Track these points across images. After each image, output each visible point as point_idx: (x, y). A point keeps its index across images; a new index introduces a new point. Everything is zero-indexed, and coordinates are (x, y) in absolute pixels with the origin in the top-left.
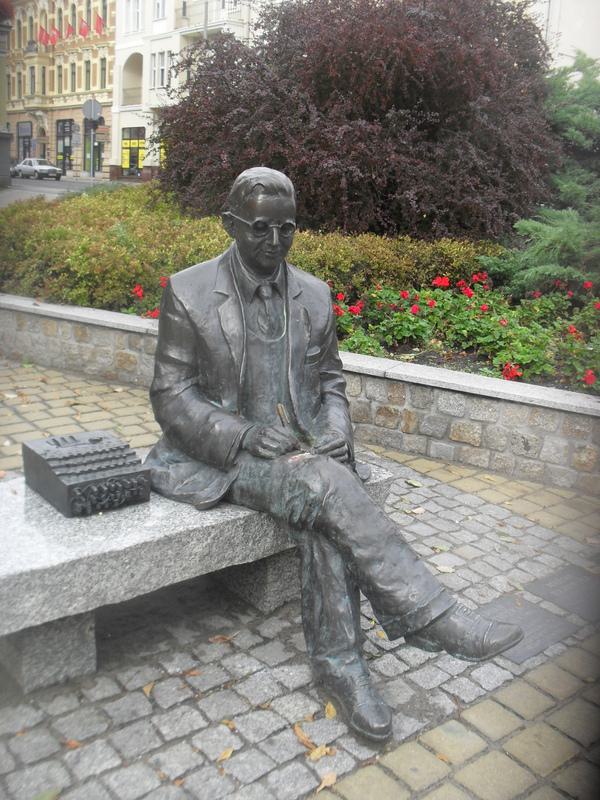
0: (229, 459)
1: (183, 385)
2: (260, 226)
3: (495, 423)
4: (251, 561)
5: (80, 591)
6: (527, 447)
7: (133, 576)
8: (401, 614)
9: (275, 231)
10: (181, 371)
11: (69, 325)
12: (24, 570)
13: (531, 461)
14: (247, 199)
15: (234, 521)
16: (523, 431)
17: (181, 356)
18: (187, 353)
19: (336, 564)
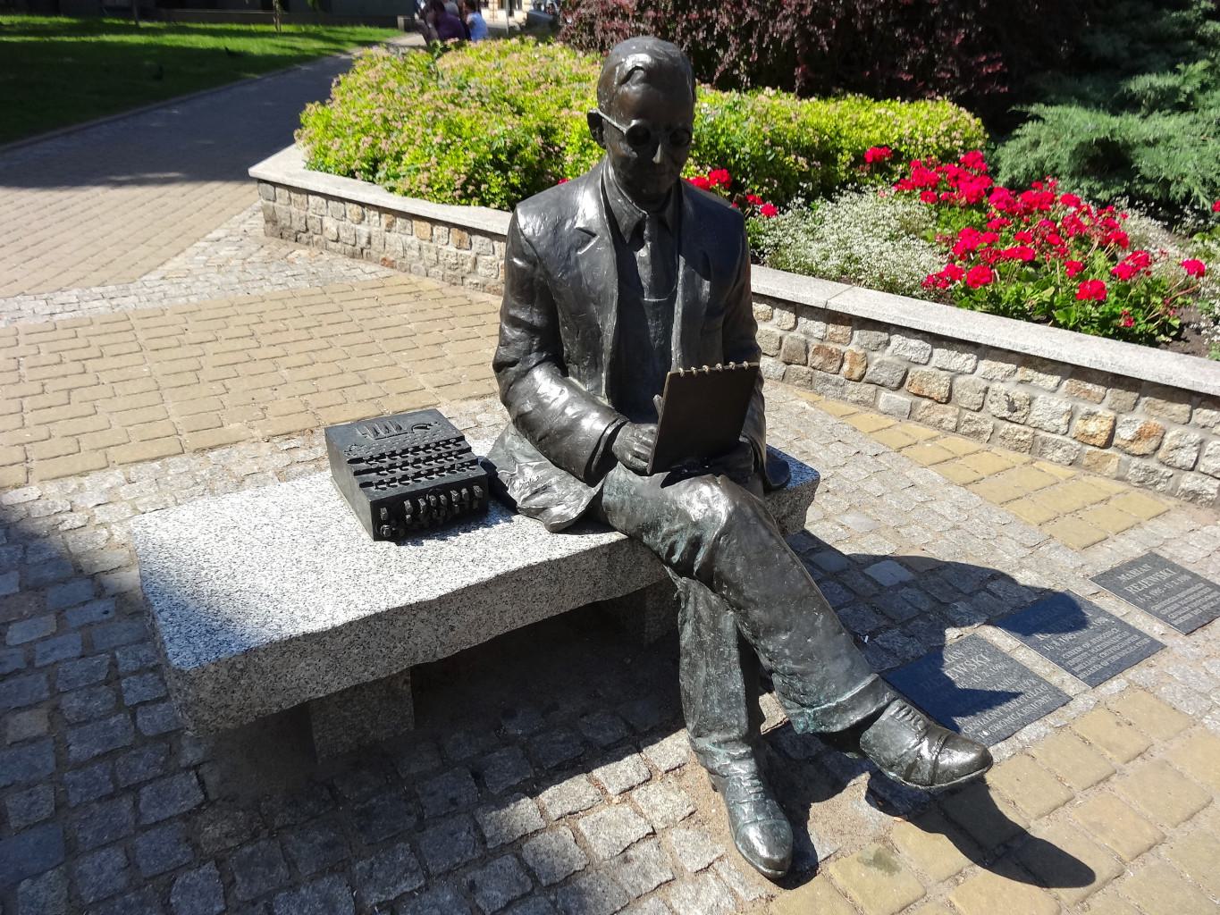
6: (1012, 408)
10: (532, 339)
12: (294, 634)
13: (1015, 425)
14: (620, 92)
18: (539, 314)
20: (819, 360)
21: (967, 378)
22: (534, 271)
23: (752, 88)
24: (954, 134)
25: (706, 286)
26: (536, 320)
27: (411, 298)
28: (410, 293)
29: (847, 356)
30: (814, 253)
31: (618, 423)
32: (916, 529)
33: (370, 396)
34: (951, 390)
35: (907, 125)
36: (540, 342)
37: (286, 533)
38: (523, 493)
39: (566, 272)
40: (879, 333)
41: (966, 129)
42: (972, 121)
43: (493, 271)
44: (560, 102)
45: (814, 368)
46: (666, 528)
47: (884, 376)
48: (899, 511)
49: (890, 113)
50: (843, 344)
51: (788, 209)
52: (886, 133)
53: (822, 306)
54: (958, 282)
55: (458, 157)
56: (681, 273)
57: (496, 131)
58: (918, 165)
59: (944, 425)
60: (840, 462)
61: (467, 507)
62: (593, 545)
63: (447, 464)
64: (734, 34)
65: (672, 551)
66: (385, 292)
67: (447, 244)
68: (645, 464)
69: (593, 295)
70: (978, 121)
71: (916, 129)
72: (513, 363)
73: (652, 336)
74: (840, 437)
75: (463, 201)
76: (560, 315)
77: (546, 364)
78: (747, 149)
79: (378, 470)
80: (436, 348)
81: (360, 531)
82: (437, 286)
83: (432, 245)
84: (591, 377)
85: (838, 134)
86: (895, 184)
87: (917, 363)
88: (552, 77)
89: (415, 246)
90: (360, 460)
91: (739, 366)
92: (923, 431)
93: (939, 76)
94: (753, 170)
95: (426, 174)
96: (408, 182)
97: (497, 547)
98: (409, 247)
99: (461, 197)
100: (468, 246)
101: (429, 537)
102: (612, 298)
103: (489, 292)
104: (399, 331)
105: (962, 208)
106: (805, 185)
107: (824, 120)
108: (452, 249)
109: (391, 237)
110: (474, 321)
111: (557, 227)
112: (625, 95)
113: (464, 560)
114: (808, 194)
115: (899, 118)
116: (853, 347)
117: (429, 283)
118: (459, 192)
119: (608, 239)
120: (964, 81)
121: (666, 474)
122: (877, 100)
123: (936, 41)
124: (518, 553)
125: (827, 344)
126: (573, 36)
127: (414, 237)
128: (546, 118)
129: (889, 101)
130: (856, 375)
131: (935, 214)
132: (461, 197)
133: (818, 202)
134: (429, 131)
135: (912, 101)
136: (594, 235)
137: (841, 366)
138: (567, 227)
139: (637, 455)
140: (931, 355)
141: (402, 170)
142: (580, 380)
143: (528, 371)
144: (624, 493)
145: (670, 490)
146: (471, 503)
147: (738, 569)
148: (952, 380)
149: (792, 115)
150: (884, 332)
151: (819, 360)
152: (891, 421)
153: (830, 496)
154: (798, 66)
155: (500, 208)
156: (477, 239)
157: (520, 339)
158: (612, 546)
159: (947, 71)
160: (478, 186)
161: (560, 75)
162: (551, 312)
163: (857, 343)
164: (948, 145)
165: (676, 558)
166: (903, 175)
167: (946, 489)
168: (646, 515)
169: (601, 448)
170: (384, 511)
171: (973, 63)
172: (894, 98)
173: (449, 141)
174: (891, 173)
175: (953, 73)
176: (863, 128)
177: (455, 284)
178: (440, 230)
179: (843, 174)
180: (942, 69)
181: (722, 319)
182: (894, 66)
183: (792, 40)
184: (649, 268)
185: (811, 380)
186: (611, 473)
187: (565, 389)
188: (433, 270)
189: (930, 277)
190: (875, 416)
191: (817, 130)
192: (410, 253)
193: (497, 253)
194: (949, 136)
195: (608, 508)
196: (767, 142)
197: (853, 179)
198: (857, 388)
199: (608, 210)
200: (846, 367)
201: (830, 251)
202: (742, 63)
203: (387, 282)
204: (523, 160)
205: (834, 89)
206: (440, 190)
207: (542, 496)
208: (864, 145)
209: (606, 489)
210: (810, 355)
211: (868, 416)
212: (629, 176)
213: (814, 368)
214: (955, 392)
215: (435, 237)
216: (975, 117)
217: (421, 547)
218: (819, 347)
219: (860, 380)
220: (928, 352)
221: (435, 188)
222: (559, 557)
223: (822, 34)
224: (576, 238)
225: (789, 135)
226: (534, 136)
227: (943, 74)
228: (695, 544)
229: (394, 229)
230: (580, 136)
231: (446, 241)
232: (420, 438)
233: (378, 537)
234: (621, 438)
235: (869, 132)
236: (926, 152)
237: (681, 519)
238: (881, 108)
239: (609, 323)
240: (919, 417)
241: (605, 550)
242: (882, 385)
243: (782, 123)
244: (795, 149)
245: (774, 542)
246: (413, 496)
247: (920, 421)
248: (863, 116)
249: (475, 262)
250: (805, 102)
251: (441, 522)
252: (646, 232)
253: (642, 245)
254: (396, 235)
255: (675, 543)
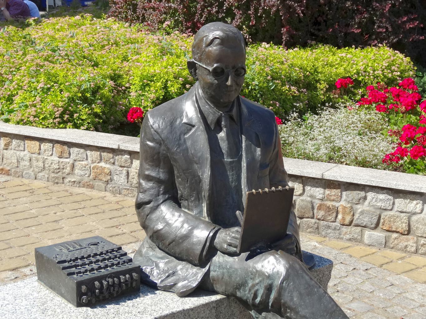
10: (160, 187)
14: (207, 49)
18: (163, 173)
20: (321, 214)
21: (419, 216)
22: (160, 147)
23: (252, 43)
24: (393, 68)
25: (258, 151)
26: (162, 176)
27: (27, 194)
28: (26, 191)
29: (340, 209)
30: (310, 147)
31: (216, 229)
32: (397, 308)
33: (17, 254)
34: (409, 225)
35: (361, 63)
36: (164, 189)
37: (22, 307)
38: (160, 278)
39: (179, 147)
40: (359, 192)
41: (401, 64)
42: (404, 59)
43: (87, 172)
44: (121, 57)
45: (319, 219)
46: (250, 283)
47: (366, 220)
48: (385, 299)
49: (349, 56)
50: (337, 201)
51: (288, 121)
52: (348, 69)
53: (320, 177)
54: (405, 158)
55: (57, 96)
56: (244, 145)
57: (83, 78)
58: (372, 89)
59: (408, 249)
60: (344, 274)
61: (129, 286)
62: (207, 301)
63: (115, 262)
64: (238, 8)
65: (255, 296)
66: (7, 191)
67: (52, 155)
68: (235, 249)
69: (195, 159)
70: (408, 59)
71: (368, 66)
72: (149, 203)
73: (230, 180)
74: (342, 261)
75: (61, 125)
76: (176, 172)
77: (168, 201)
78: (256, 82)
79: (76, 266)
80: (55, 224)
81: (67, 304)
82: (44, 185)
83: (40, 156)
84: (196, 207)
85: (316, 70)
86: (357, 102)
87: (386, 210)
88: (112, 41)
89: (27, 158)
90: (64, 262)
91: (284, 188)
92: (395, 254)
93: (378, 31)
94: (261, 96)
95: (34, 109)
96: (20, 115)
97: (151, 306)
98: (22, 159)
99: (60, 123)
100: (67, 155)
101: (109, 304)
102: (207, 159)
103: (83, 187)
104: (26, 215)
105: (403, 113)
106: (298, 105)
107: (305, 62)
108: (55, 158)
109: (7, 153)
110: (76, 206)
111: (172, 123)
112: (210, 52)
113: (134, 313)
114: (300, 110)
115: (355, 58)
116: (343, 203)
117: (37, 184)
118: (58, 120)
119: (202, 127)
120: (396, 34)
121: (248, 253)
122: (339, 48)
123: (374, 9)
124: (164, 307)
125: (326, 203)
126: (120, 13)
127: (26, 152)
128: (114, 68)
129: (347, 48)
130: (347, 221)
131: (387, 119)
132: (60, 123)
133: (308, 115)
134: (33, 80)
135: (363, 48)
136: (194, 126)
137: (337, 216)
138: (178, 122)
139: (230, 245)
140: (394, 204)
141: (15, 106)
142: (189, 209)
143: (158, 206)
144: (223, 268)
145: (250, 262)
146: (132, 284)
147: (295, 299)
148: (409, 218)
149: (284, 60)
150: (362, 191)
151: (321, 214)
152: (374, 250)
153: (339, 294)
154: (283, 26)
155: (87, 129)
156: (74, 150)
157: (152, 188)
158: (217, 302)
159: (383, 27)
160: (72, 116)
161: (118, 39)
162: (170, 172)
163: (346, 200)
164: (390, 75)
165: (258, 300)
166: (363, 96)
167: (414, 286)
168: (238, 278)
169: (208, 244)
170: (84, 288)
171: (400, 22)
172: (350, 46)
173: (49, 86)
174: (354, 94)
175: (387, 28)
176: (332, 66)
177: (57, 183)
178: (46, 146)
179: (322, 97)
180: (379, 27)
181: (268, 169)
182: (348, 25)
183: (278, 11)
184: (226, 142)
185: (318, 228)
186: (214, 258)
187: (182, 214)
188: (41, 174)
189: (387, 156)
190: (363, 247)
191: (301, 69)
192: (22, 163)
193: (89, 159)
194: (390, 69)
195: (214, 280)
196: (269, 78)
197: (329, 100)
198: (349, 230)
199: (201, 112)
200: (340, 216)
201: (319, 145)
202: (244, 26)
203: (6, 184)
204: (103, 96)
205: (309, 41)
206: (43, 119)
207: (172, 278)
208: (334, 77)
209: (212, 268)
210: (315, 211)
211: (358, 248)
212: (213, 93)
213: (319, 219)
214: (412, 226)
215: (42, 151)
216: (406, 57)
217: (105, 309)
218: (321, 205)
219: (350, 224)
220: (392, 202)
221: (41, 118)
222: (189, 308)
223: (298, 6)
224: (183, 128)
225: (283, 72)
226: (108, 80)
227: (381, 30)
228: (269, 289)
229: (10, 147)
230: (141, 79)
231: (51, 153)
232: (94, 250)
233: (80, 304)
234: (219, 237)
235: (336, 68)
236: (376, 80)
237: (259, 276)
238: (343, 53)
239: (206, 174)
240: (392, 246)
241: (214, 305)
242: (365, 227)
243: (277, 65)
244: (288, 82)
245: (313, 282)
246: (100, 279)
247: (392, 248)
248: (331, 58)
249: (73, 166)
250: (291, 51)
251: (115, 295)
252: (223, 123)
253: (221, 130)
254: (12, 151)
255: (257, 290)
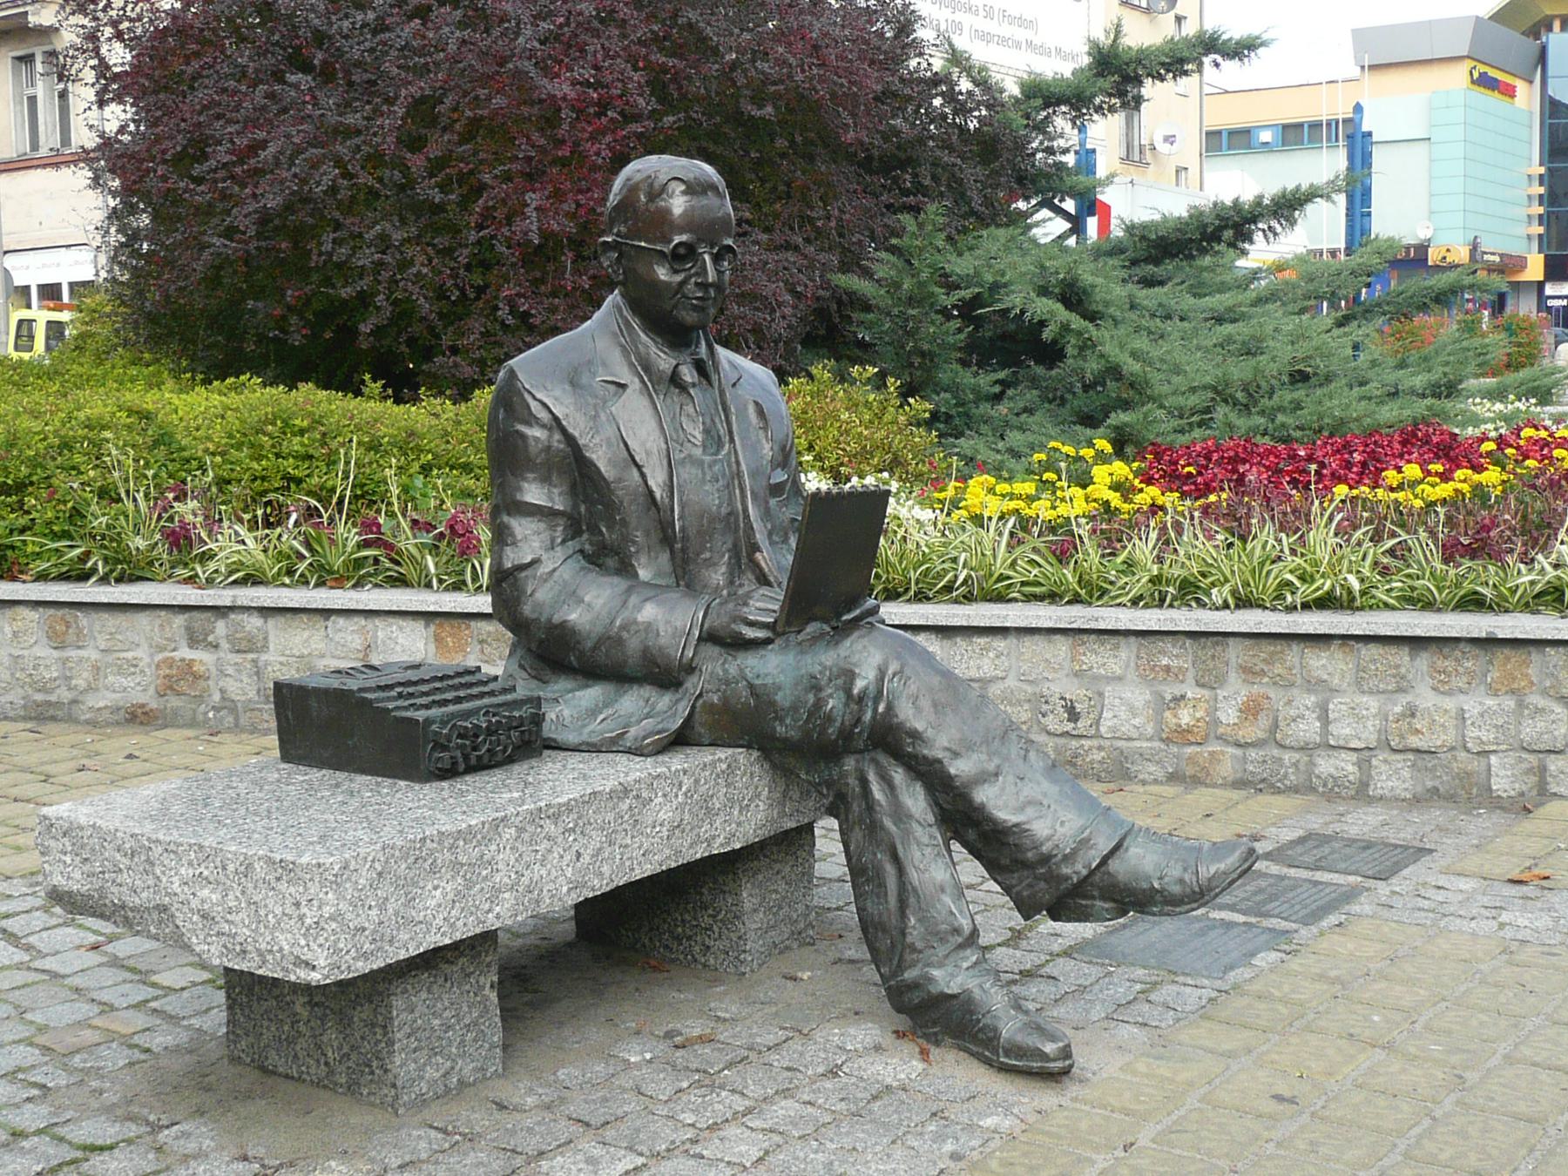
0: (684, 660)
1: (560, 553)
2: (682, 251)
3: (1003, 679)
4: (738, 846)
5: (506, 880)
6: (1073, 716)
7: (579, 855)
8: (1046, 859)
9: (707, 257)
10: (552, 528)
11: (33, 615)
15: (713, 764)
16: (1062, 686)
17: (552, 500)
19: (916, 801)
